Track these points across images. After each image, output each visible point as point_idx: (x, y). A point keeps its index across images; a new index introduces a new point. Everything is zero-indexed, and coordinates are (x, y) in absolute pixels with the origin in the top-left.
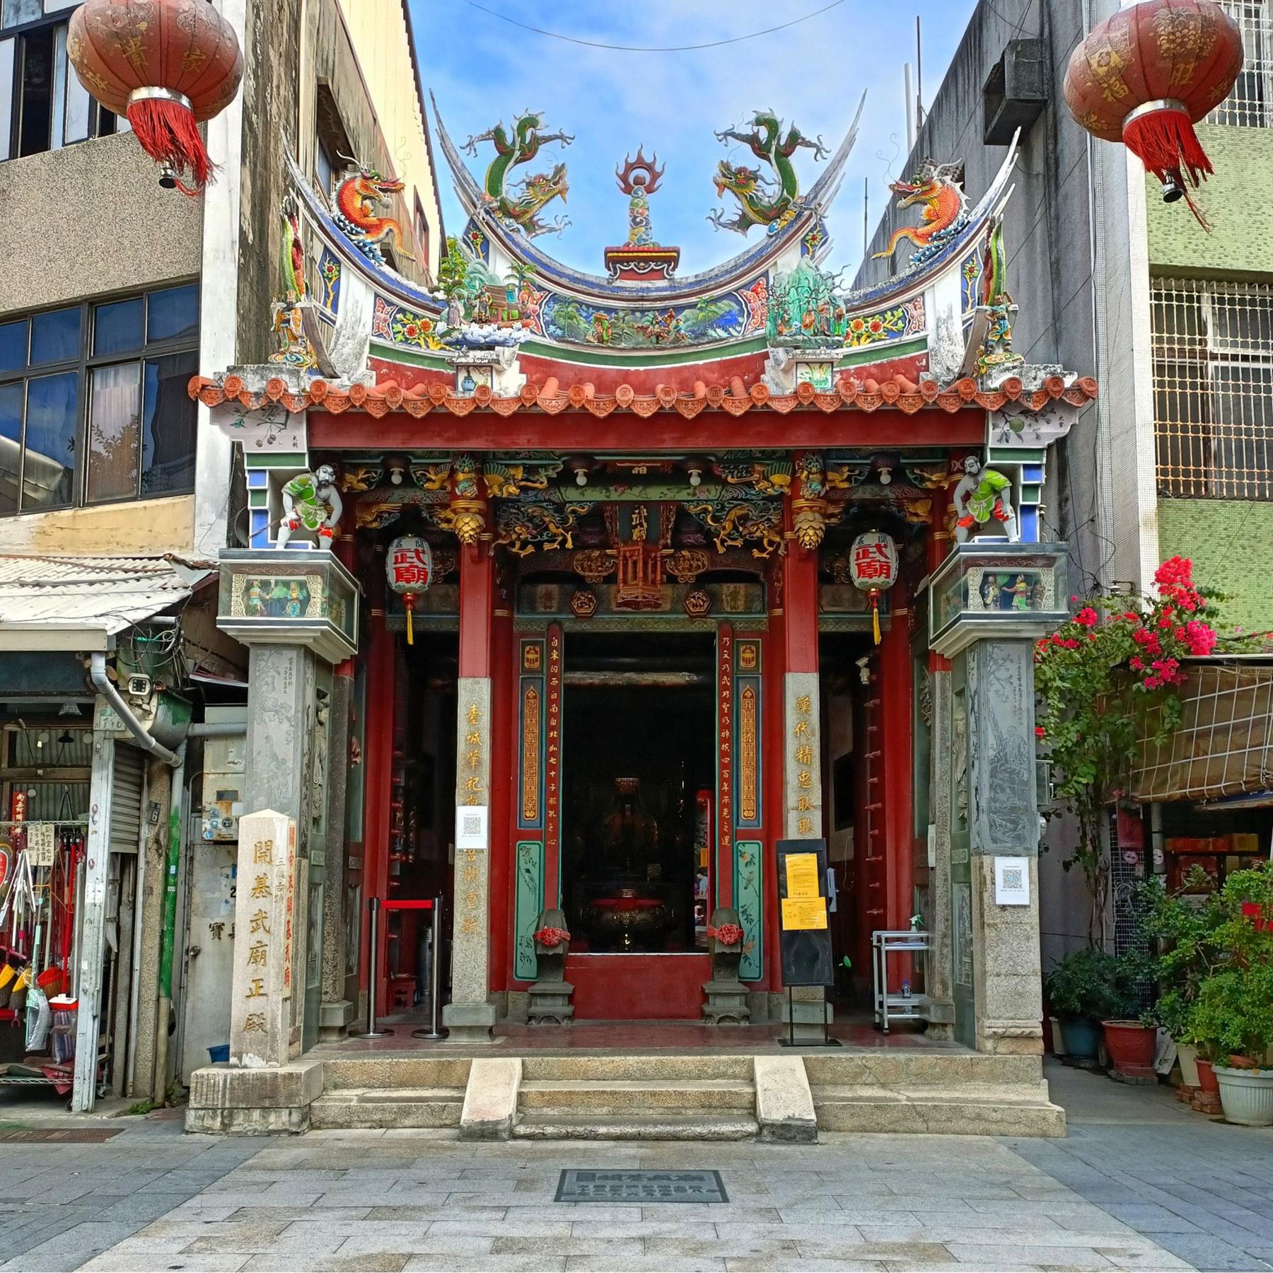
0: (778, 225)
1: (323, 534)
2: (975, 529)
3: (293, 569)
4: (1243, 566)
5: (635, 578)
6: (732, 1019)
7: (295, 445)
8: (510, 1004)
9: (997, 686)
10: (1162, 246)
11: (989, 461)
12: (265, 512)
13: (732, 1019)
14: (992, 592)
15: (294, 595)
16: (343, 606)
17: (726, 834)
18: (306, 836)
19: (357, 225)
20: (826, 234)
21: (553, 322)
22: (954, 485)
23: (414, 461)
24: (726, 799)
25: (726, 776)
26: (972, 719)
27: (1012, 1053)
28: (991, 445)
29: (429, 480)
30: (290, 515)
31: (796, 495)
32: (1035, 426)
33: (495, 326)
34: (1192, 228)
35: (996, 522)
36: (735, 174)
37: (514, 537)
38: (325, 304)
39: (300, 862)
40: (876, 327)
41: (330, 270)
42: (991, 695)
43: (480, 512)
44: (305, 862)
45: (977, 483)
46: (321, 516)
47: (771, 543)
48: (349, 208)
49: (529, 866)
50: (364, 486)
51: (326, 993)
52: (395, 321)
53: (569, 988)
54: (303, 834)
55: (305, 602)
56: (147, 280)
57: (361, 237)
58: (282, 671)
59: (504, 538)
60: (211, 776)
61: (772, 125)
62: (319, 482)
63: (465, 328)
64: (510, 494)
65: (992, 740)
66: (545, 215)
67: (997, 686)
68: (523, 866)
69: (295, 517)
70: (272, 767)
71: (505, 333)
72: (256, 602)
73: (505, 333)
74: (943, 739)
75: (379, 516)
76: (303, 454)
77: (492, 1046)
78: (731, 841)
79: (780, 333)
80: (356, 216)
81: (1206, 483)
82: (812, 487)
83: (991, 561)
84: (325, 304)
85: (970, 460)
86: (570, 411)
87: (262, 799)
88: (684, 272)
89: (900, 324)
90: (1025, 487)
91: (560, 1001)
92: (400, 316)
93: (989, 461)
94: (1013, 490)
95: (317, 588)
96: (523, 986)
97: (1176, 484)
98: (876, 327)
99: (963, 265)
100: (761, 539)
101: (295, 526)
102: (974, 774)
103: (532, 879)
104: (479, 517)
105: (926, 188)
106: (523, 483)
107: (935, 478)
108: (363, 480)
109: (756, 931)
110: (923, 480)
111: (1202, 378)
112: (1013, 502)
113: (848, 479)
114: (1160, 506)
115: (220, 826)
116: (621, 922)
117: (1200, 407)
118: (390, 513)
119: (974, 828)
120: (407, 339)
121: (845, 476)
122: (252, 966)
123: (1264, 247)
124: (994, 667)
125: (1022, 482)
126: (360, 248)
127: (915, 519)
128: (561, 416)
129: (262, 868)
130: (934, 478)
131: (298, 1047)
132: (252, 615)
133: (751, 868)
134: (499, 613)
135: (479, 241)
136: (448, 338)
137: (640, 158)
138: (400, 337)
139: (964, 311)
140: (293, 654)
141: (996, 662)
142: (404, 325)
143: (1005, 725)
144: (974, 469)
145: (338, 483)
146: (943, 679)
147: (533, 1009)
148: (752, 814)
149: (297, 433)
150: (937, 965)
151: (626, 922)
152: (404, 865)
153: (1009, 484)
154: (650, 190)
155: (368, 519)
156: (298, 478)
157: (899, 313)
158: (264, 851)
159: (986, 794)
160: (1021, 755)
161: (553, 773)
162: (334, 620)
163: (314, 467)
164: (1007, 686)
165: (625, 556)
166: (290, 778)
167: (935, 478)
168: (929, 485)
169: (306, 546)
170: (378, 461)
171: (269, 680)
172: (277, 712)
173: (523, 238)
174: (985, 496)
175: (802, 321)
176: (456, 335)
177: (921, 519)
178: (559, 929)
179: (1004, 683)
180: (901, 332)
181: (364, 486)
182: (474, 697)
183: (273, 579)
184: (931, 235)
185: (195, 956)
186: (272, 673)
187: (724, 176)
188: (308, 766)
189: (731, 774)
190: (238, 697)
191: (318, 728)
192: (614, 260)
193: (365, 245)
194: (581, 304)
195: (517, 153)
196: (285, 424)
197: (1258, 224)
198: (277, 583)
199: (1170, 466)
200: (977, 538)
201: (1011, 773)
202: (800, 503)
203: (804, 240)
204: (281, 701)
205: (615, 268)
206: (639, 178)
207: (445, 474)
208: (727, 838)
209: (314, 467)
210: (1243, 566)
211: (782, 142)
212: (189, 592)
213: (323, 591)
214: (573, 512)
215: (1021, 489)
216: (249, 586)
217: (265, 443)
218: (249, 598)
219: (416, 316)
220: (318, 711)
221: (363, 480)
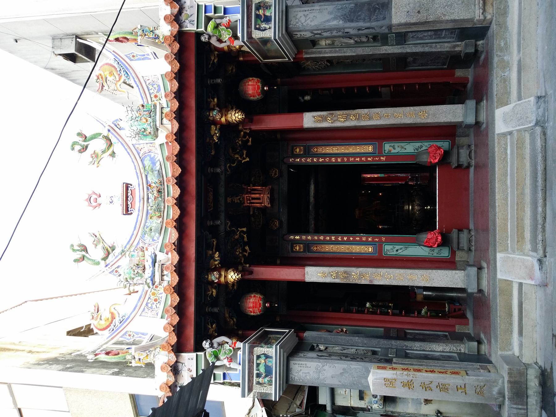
0: (113, 140)
1: (235, 346)
2: (235, 37)
3: (251, 361)
5: (259, 199)
6: (470, 152)
7: (192, 359)
8: (462, 259)
9: (309, 22)
11: (203, 29)
12: (224, 374)
13: (470, 152)
14: (264, 25)
15: (263, 361)
16: (271, 336)
17: (380, 158)
18: (381, 359)
19: (111, 323)
20: (117, 120)
23: (203, 301)
24: (363, 159)
25: (353, 159)
26: (325, 34)
27: (492, 5)
28: (195, 29)
30: (226, 362)
32: (187, 8)
35: (232, 27)
37: (241, 255)
38: (144, 338)
39: (395, 363)
40: (156, 96)
42: (313, 24)
43: (226, 271)
44: (394, 360)
45: (213, 36)
46: (227, 347)
47: (244, 136)
48: (104, 326)
49: (395, 250)
51: (460, 350)
52: (151, 308)
53: (455, 231)
54: (380, 361)
55: (267, 357)
58: (300, 368)
59: (241, 260)
60: (352, 403)
61: (75, 143)
62: (210, 347)
65: (334, 23)
66: (109, 242)
67: (309, 22)
68: (395, 253)
69: (226, 359)
70: (347, 375)
72: (266, 380)
74: (336, 52)
75: (231, 317)
76: (197, 355)
77: (488, 268)
78: (383, 156)
80: (108, 323)
82: (215, 114)
83: (249, 26)
84: (144, 338)
85: (203, 39)
87: (363, 381)
88: (134, 181)
89: (155, 86)
90: (215, 13)
91: (461, 235)
92: (150, 305)
93: (203, 29)
95: (258, 350)
96: (453, 253)
98: (156, 96)
99: (131, 60)
100: (242, 141)
101: (231, 360)
102: (352, 32)
103: (401, 249)
104: (229, 271)
105: (100, 77)
108: (212, 326)
109: (426, 144)
112: (221, 18)
115: (376, 399)
116: (419, 210)
118: (230, 312)
119: (378, 30)
122: (450, 391)
124: (300, 23)
125: (213, 13)
127: (234, 70)
129: (398, 383)
130: (213, 58)
131: (489, 366)
132: (272, 382)
133: (396, 147)
134: (278, 262)
138: (158, 305)
139: (150, 59)
140: (292, 363)
141: (297, 23)
142: (153, 304)
143: (328, 17)
144: (207, 37)
145: (211, 338)
146: (307, 53)
147: (466, 248)
148: (370, 147)
149: (187, 358)
150: (446, 50)
151: (419, 208)
152: (394, 308)
155: (232, 322)
156: (208, 358)
157: (150, 87)
158: (389, 382)
159: (361, 24)
160: (342, 8)
161: (351, 239)
162: (277, 340)
163: (203, 350)
164: (309, 17)
165: (249, 203)
166: (352, 367)
169: (240, 354)
170: (203, 318)
171: (304, 375)
172: (319, 372)
174: (220, 32)
176: (149, 281)
177: (234, 67)
178: (425, 237)
180: (159, 86)
182: (314, 274)
183: (255, 372)
185: (441, 413)
186: (301, 373)
188: (347, 357)
189: (352, 157)
190: (313, 391)
191: (328, 350)
192: (127, 211)
196: (182, 364)
198: (258, 370)
201: (351, 13)
202: (223, 119)
204: (314, 370)
207: (210, 287)
209: (203, 350)
211: (81, 139)
213: (262, 347)
214: (229, 227)
215: (216, 15)
216: (258, 383)
219: (149, 298)
220: (320, 351)
221: (212, 326)
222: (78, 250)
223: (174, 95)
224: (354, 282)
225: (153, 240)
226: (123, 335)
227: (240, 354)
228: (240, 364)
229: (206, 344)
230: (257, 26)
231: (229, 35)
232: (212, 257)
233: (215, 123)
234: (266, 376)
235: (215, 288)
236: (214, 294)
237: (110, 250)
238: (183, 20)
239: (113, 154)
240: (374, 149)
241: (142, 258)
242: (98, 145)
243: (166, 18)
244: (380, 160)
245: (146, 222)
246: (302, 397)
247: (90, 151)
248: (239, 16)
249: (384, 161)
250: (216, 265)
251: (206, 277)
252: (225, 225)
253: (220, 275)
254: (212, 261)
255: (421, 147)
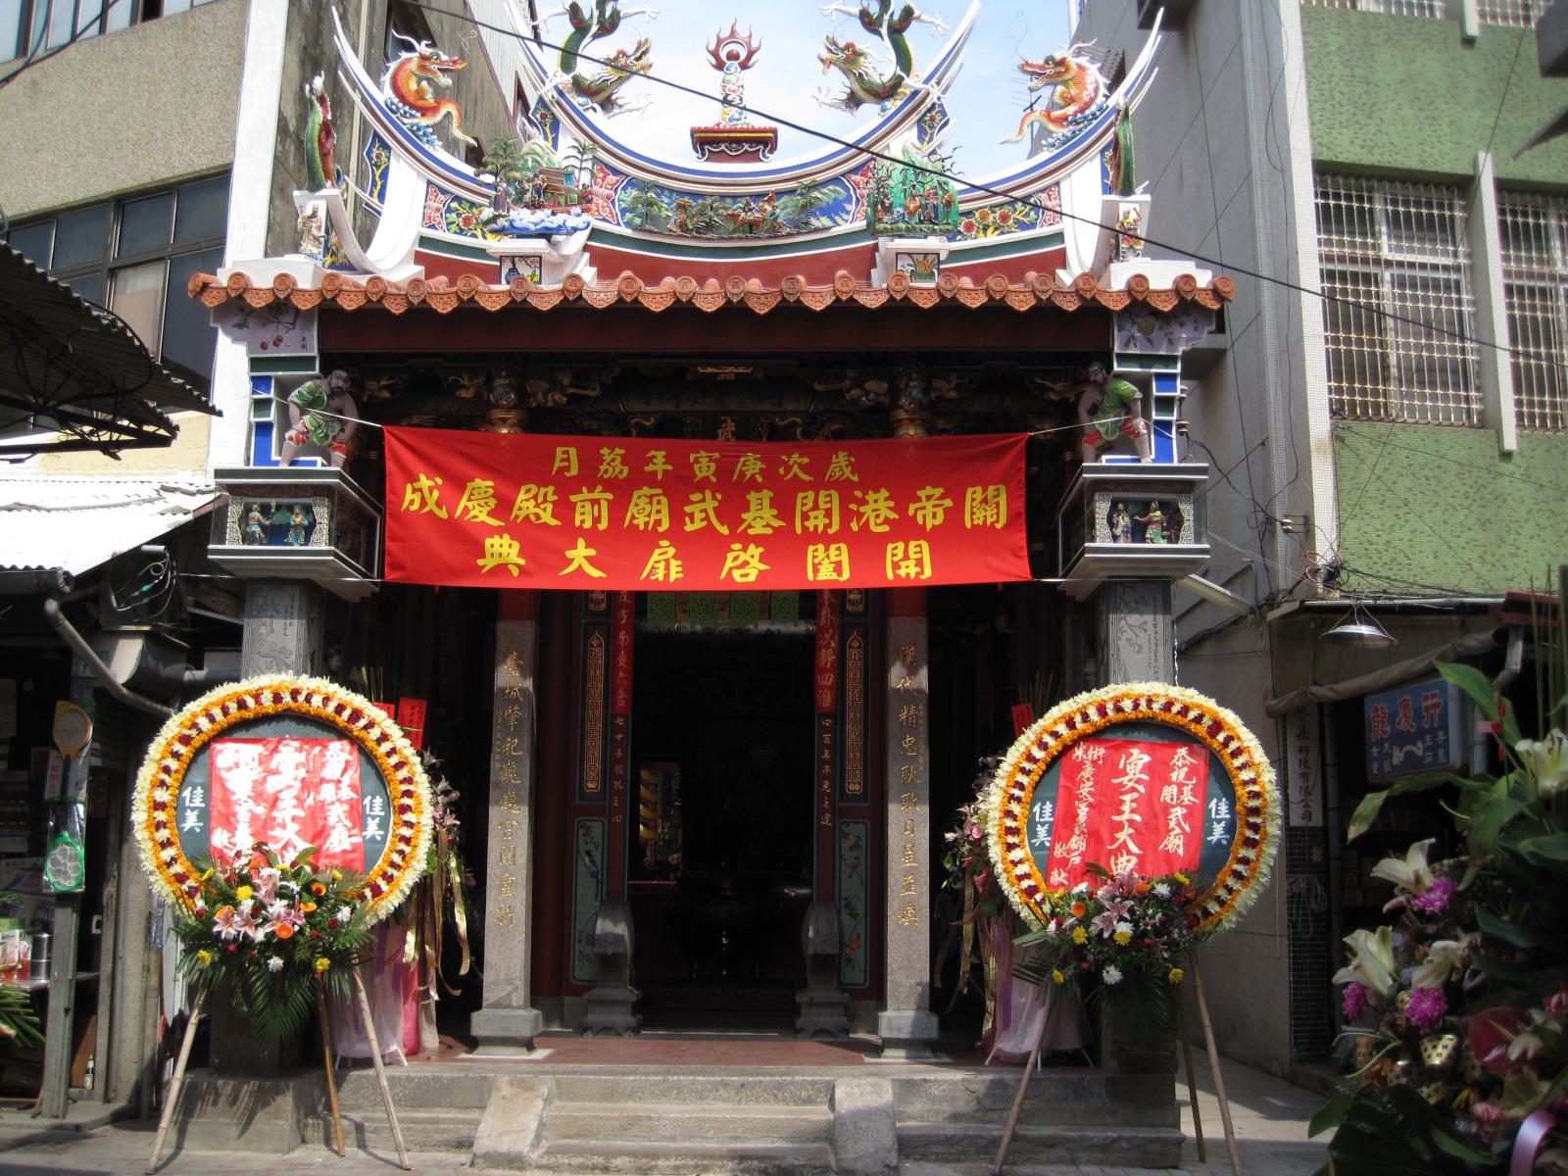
0: (892, 105)
4: (1427, 499)
9: (1128, 634)
10: (1326, 140)
14: (1123, 521)
15: (298, 520)
19: (412, 107)
20: (944, 114)
21: (632, 210)
22: (1079, 395)
25: (827, 741)
28: (1117, 350)
29: (463, 387)
31: (895, 406)
33: (549, 212)
34: (1358, 122)
35: (1127, 442)
36: (842, 50)
38: (371, 194)
41: (378, 156)
42: (1123, 643)
48: (404, 91)
49: (591, 847)
50: (386, 395)
52: (449, 210)
55: (309, 530)
56: (177, 172)
57: (415, 121)
63: (513, 214)
64: (555, 401)
67: (1128, 634)
68: (583, 847)
71: (559, 219)
72: (256, 529)
73: (559, 219)
79: (880, 220)
80: (411, 99)
81: (1386, 404)
84: (371, 194)
86: (621, 305)
92: (454, 205)
93: (1116, 368)
94: (1146, 401)
97: (1352, 404)
106: (571, 391)
107: (1058, 390)
109: (861, 929)
110: (1046, 389)
111: (1377, 285)
113: (958, 388)
114: (1334, 428)
117: (1372, 318)
120: (462, 230)
121: (954, 384)
123: (1437, 145)
126: (413, 132)
128: (610, 310)
130: (1058, 387)
135: (548, 121)
136: (493, 226)
137: (733, 33)
138: (454, 227)
140: (296, 591)
148: (857, 787)
153: (1139, 395)
154: (744, 66)
161: (619, 736)
163: (326, 371)
164: (1141, 634)
167: (1058, 390)
168: (1053, 397)
172: (274, 658)
173: (598, 118)
175: (906, 208)
176: (502, 222)
179: (1137, 630)
180: (1032, 225)
181: (386, 395)
183: (273, 502)
184: (1066, 119)
187: (830, 51)
189: (833, 739)
192: (706, 141)
193: (419, 129)
194: (663, 188)
195: (594, 28)
196: (294, 324)
197: (1430, 121)
199: (1345, 384)
200: (1104, 457)
203: (920, 121)
205: (703, 150)
206: (731, 55)
207: (480, 380)
208: (828, 816)
210: (1427, 499)
211: (896, 17)
212: (190, 517)
214: (638, 424)
216: (248, 510)
217: (271, 345)
218: (248, 525)
221: (386, 387)
222: (602, 13)
223: (949, 295)
224: (496, 743)
225: (623, 211)
226: (381, 140)
227: (314, 463)
228: (293, 463)
229: (339, 378)
230: (1121, 506)
231: (1106, 433)
232: (555, 386)
233: (894, 392)
234: (263, 527)
235: (478, 395)
236: (464, 394)
237: (602, 96)
238: (1138, 320)
239: (853, 101)
240: (855, 797)
241: (562, 200)
242: (880, 62)
243: (1140, 279)
244: (823, 811)
245: (672, 191)
246: (222, 609)
247: (864, 40)
248: (1147, 461)
249: (819, 820)
250: (534, 395)
251: (504, 374)
252: (643, 413)
253: (509, 409)
254: (546, 386)
255: (854, 916)
